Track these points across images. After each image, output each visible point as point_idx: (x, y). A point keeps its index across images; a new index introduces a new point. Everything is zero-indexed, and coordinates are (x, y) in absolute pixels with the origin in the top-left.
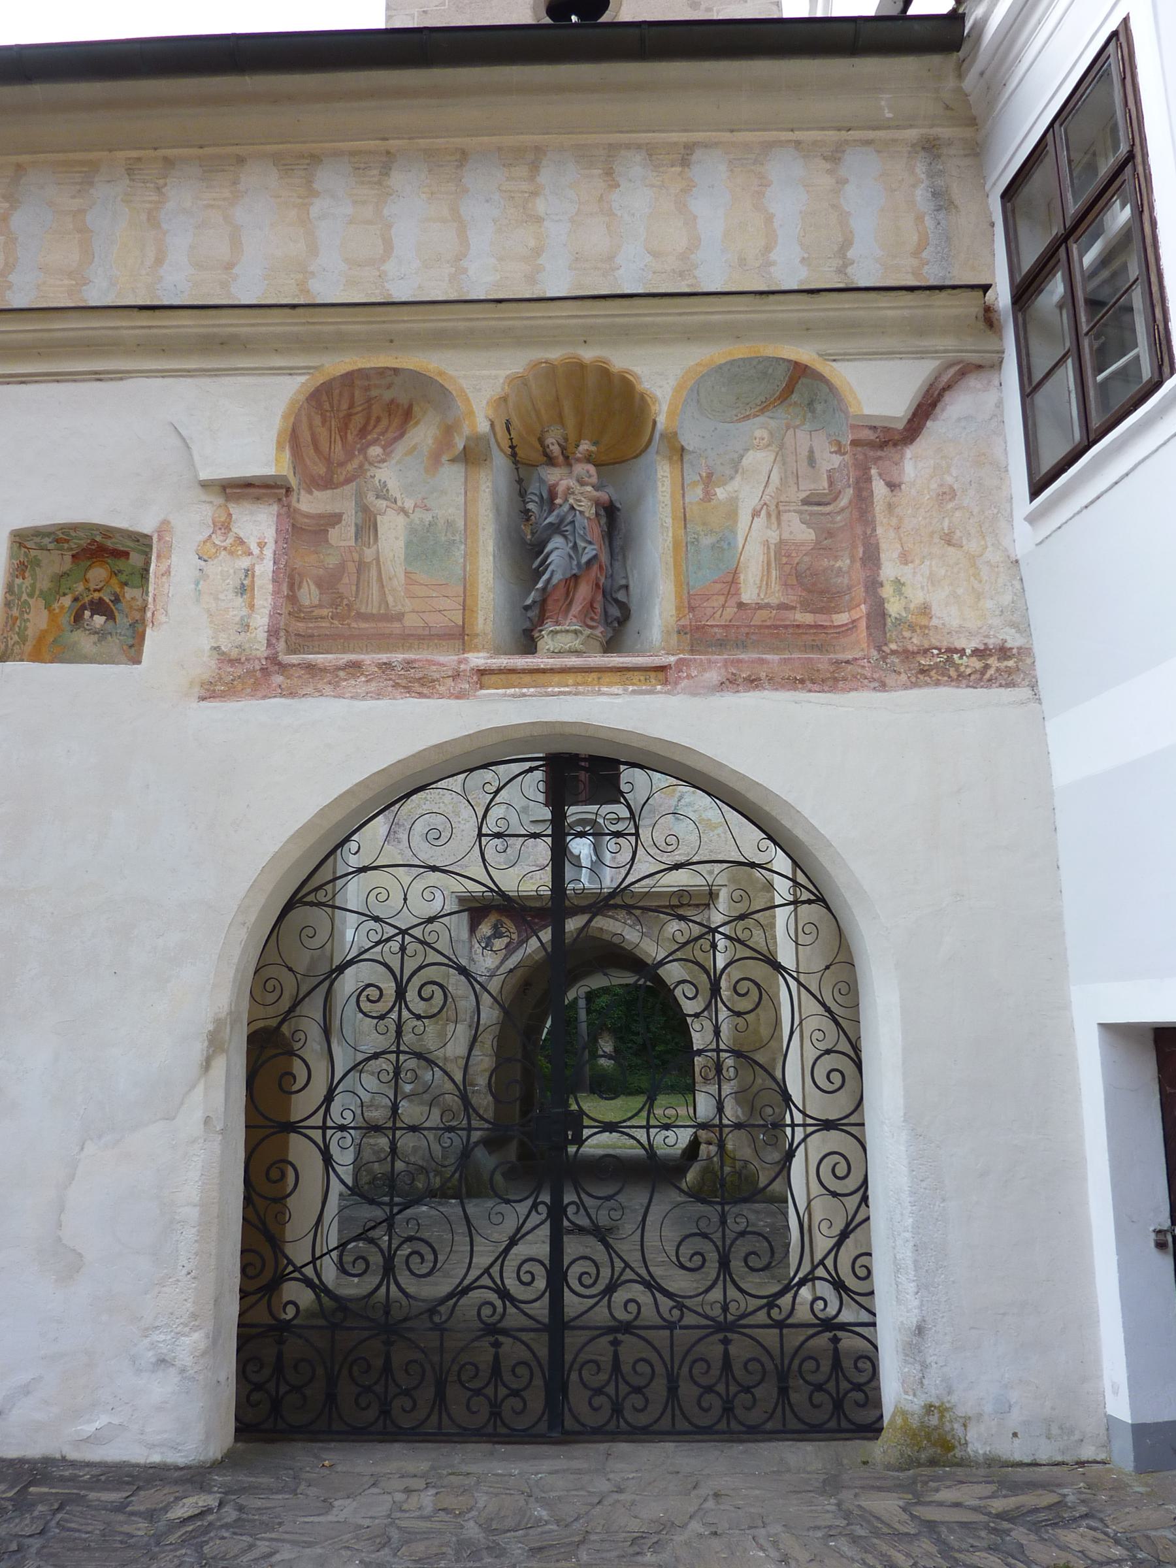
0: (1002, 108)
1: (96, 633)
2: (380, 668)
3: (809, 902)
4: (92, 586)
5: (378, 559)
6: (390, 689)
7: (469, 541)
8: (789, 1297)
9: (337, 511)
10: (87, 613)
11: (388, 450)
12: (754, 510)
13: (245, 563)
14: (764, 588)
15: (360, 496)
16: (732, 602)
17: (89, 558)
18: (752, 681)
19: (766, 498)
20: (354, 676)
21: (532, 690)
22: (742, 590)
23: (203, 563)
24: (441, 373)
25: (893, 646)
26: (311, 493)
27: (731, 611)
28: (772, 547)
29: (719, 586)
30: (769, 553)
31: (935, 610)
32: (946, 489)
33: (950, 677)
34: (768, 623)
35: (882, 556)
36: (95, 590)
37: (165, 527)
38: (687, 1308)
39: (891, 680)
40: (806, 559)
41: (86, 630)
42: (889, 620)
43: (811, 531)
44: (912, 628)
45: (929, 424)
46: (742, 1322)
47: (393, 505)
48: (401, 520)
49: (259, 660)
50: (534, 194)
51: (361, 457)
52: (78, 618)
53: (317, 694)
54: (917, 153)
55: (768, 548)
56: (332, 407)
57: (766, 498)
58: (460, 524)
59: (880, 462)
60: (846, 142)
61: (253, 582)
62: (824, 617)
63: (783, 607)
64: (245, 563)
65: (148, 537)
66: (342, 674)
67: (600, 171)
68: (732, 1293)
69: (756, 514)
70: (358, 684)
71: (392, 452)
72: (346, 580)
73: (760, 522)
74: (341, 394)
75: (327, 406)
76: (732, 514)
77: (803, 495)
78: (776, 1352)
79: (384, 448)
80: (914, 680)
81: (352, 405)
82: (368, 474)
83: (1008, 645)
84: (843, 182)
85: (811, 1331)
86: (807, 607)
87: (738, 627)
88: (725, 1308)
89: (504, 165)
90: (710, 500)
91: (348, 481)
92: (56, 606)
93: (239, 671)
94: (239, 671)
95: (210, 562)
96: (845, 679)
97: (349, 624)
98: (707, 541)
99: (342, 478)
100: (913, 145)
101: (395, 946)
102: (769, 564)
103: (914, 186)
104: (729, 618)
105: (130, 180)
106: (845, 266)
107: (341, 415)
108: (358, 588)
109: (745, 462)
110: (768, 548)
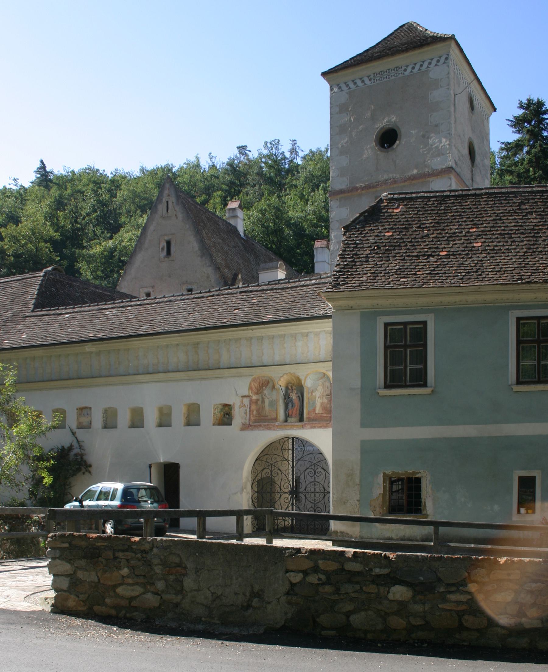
13: (245, 408)
15: (262, 396)
27: (314, 414)
37: (234, 404)
52: (225, 415)
63: (322, 413)
69: (319, 398)
73: (319, 399)
76: (315, 398)
86: (326, 413)
91: (261, 393)
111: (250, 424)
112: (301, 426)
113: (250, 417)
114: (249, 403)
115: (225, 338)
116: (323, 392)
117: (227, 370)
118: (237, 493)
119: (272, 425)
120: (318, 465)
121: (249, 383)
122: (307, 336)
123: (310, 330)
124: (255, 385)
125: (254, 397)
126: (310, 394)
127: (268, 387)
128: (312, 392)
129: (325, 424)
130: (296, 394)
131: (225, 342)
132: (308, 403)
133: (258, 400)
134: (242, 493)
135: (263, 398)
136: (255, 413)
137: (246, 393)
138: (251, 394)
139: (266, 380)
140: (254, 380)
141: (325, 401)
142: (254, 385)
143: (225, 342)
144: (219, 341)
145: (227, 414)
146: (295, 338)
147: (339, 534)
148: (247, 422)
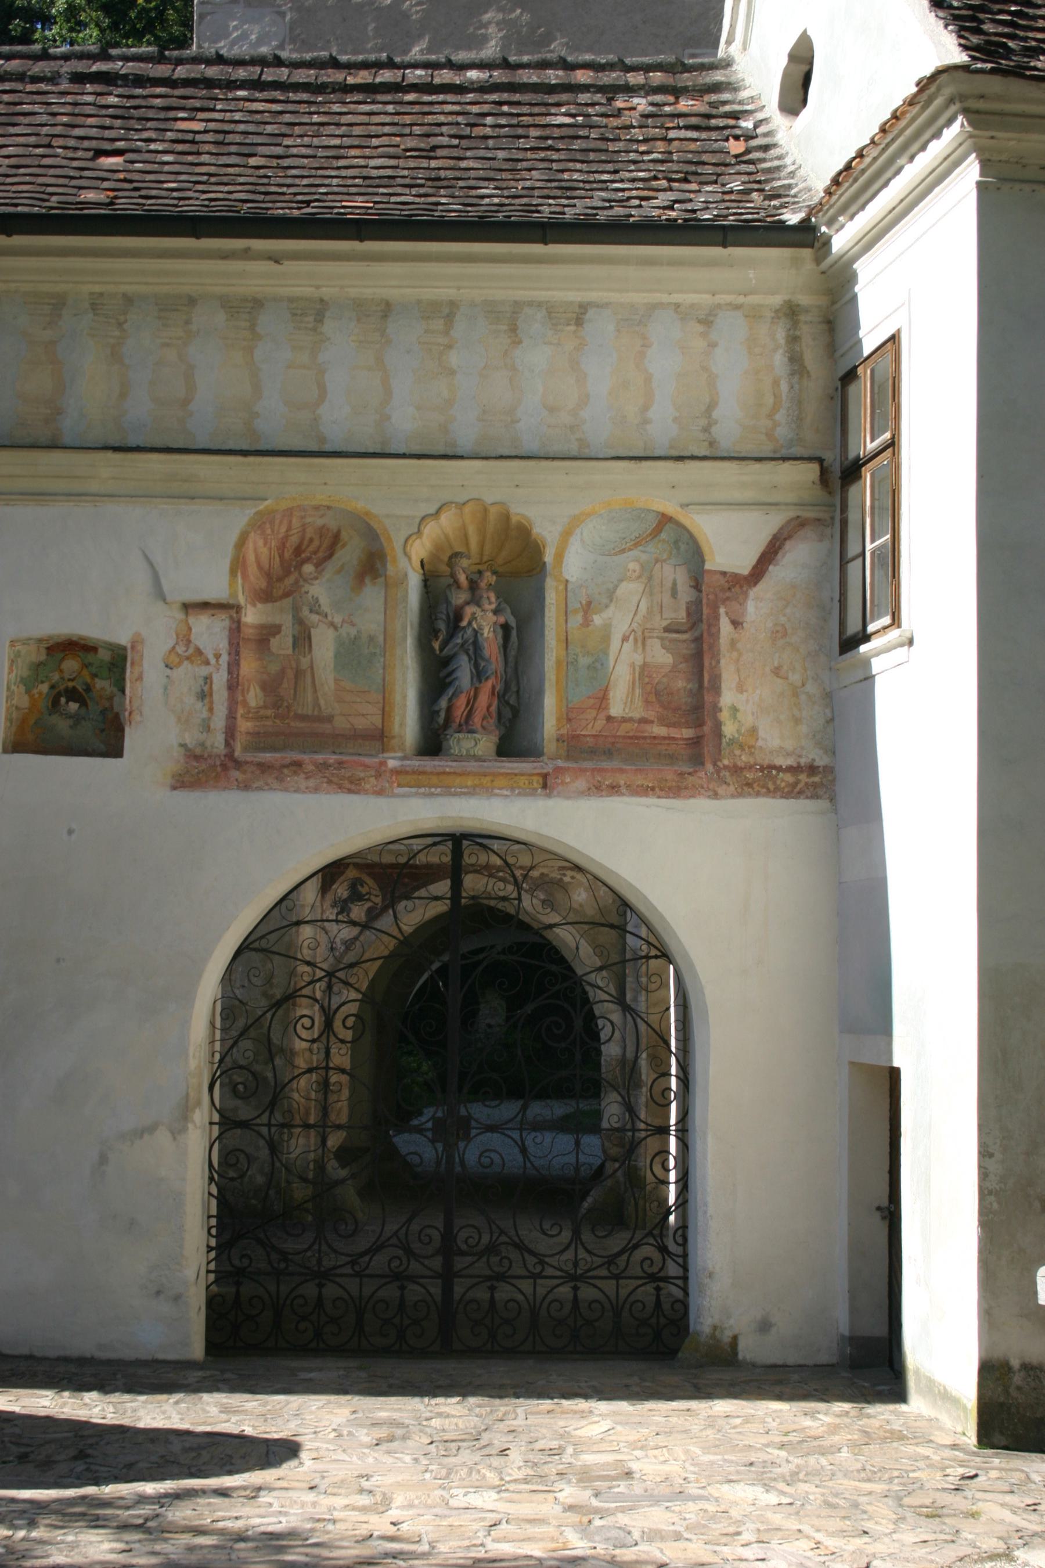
0: (846, 303)
1: (71, 717)
2: (317, 767)
3: (656, 957)
4: (67, 676)
5: (312, 668)
6: (325, 785)
7: (387, 654)
8: (624, 1257)
9: (277, 622)
10: (63, 700)
11: (320, 568)
12: (624, 636)
13: (204, 671)
14: (629, 704)
15: (296, 610)
16: (602, 716)
17: (63, 651)
18: (613, 787)
19: (635, 625)
20: (295, 773)
21: (439, 790)
22: (611, 705)
23: (168, 671)
24: (367, 513)
25: (726, 762)
26: (254, 605)
27: (601, 723)
28: (637, 668)
29: (592, 701)
30: (634, 673)
31: (761, 733)
32: (779, 628)
33: (768, 789)
34: (631, 734)
35: (723, 686)
36: (69, 680)
37: (137, 642)
38: (548, 1264)
39: (721, 790)
40: (665, 680)
41: (62, 714)
42: (724, 740)
43: (670, 655)
44: (742, 747)
45: (771, 568)
46: (591, 1274)
47: (324, 620)
48: (331, 633)
49: (219, 756)
50: (450, 347)
51: (296, 574)
52: (55, 703)
53: (266, 787)
54: (779, 318)
55: (634, 669)
56: (273, 531)
57: (635, 625)
58: (381, 638)
59: (728, 603)
60: (719, 306)
61: (211, 688)
62: (676, 730)
63: (643, 721)
64: (204, 671)
65: (125, 648)
66: (286, 771)
67: (505, 327)
68: (582, 1254)
69: (625, 639)
70: (300, 780)
71: (323, 570)
72: (285, 685)
73: (628, 646)
74: (281, 522)
75: (269, 531)
76: (606, 638)
77: (665, 623)
78: (613, 1297)
79: (317, 566)
80: (739, 790)
81: (289, 529)
82: (303, 590)
83: (816, 764)
84: (713, 345)
85: (640, 1282)
86: (663, 721)
87: (606, 737)
88: (576, 1264)
89: (422, 318)
90: (588, 626)
91: (286, 595)
92: (35, 691)
93: (203, 766)
94: (203, 766)
95: (175, 670)
96: (686, 788)
97: (288, 724)
98: (584, 661)
99: (281, 592)
100: (777, 311)
101: (323, 984)
102: (634, 683)
103: (775, 350)
104: (599, 729)
105: (95, 315)
106: (710, 425)
107: (280, 536)
108: (295, 692)
109: (619, 592)
110: (634, 669)
111: (230, 756)
112: (537, 781)
113: (231, 716)
114: (223, 645)
115: (97, 289)
116: (650, 611)
117: (110, 455)
118: (151, 1129)
119: (366, 766)
120: (346, 983)
121: (233, 537)
122: (579, 322)
123: (593, 296)
124: (259, 549)
125: (252, 616)
126: (576, 620)
127: (330, 567)
128: (588, 608)
129: (670, 776)
130: (496, 612)
131: (94, 307)
132: (568, 664)
133: (273, 630)
134: (184, 1130)
135: (299, 621)
136: (254, 697)
137: (217, 588)
138: (242, 600)
139: (322, 531)
140: (260, 523)
141: (661, 656)
142: (255, 550)
143: (94, 307)
144: (58, 303)
145: (72, 694)
146: (513, 329)
147: (1017, 1379)
148: (218, 741)
